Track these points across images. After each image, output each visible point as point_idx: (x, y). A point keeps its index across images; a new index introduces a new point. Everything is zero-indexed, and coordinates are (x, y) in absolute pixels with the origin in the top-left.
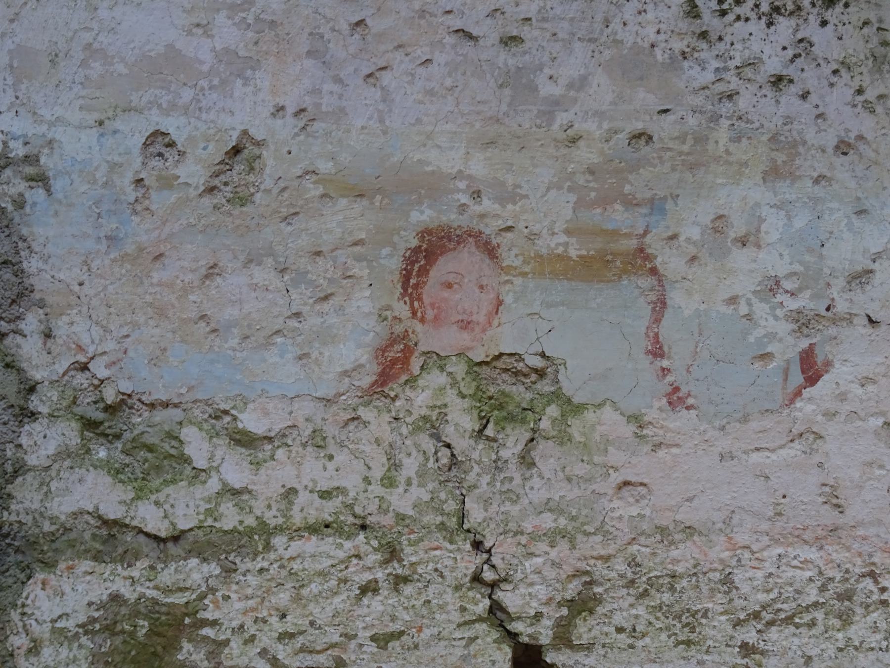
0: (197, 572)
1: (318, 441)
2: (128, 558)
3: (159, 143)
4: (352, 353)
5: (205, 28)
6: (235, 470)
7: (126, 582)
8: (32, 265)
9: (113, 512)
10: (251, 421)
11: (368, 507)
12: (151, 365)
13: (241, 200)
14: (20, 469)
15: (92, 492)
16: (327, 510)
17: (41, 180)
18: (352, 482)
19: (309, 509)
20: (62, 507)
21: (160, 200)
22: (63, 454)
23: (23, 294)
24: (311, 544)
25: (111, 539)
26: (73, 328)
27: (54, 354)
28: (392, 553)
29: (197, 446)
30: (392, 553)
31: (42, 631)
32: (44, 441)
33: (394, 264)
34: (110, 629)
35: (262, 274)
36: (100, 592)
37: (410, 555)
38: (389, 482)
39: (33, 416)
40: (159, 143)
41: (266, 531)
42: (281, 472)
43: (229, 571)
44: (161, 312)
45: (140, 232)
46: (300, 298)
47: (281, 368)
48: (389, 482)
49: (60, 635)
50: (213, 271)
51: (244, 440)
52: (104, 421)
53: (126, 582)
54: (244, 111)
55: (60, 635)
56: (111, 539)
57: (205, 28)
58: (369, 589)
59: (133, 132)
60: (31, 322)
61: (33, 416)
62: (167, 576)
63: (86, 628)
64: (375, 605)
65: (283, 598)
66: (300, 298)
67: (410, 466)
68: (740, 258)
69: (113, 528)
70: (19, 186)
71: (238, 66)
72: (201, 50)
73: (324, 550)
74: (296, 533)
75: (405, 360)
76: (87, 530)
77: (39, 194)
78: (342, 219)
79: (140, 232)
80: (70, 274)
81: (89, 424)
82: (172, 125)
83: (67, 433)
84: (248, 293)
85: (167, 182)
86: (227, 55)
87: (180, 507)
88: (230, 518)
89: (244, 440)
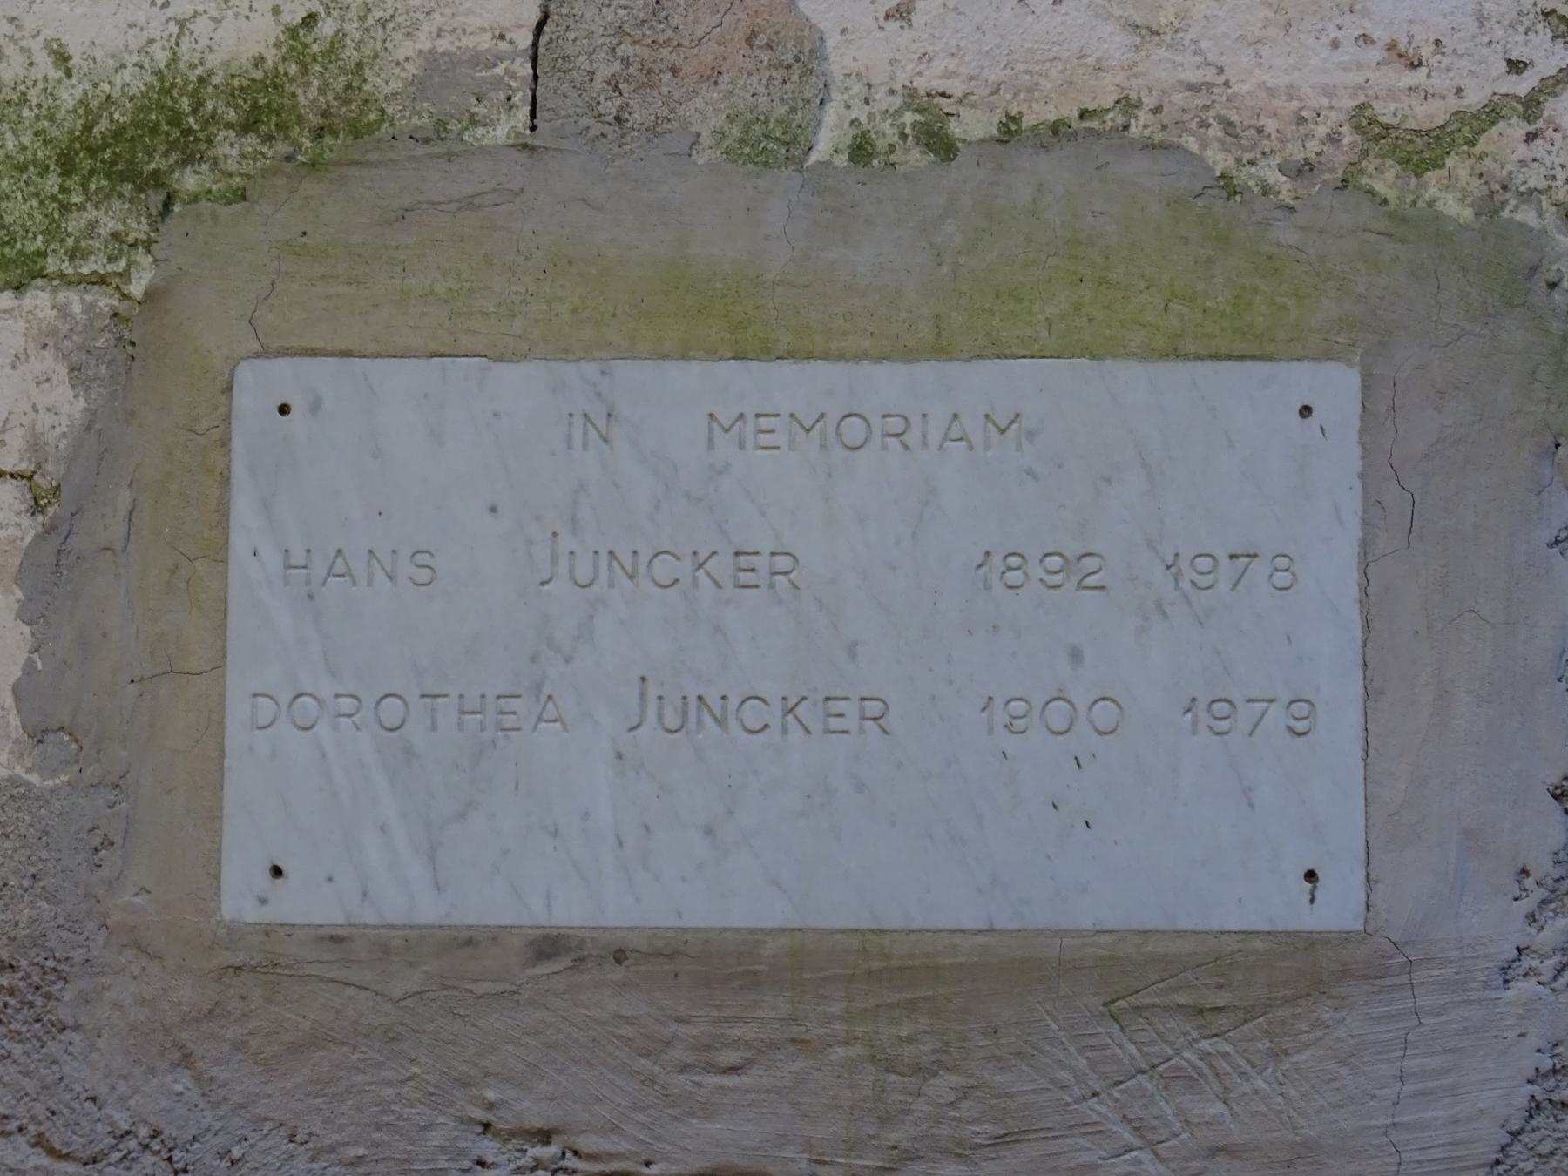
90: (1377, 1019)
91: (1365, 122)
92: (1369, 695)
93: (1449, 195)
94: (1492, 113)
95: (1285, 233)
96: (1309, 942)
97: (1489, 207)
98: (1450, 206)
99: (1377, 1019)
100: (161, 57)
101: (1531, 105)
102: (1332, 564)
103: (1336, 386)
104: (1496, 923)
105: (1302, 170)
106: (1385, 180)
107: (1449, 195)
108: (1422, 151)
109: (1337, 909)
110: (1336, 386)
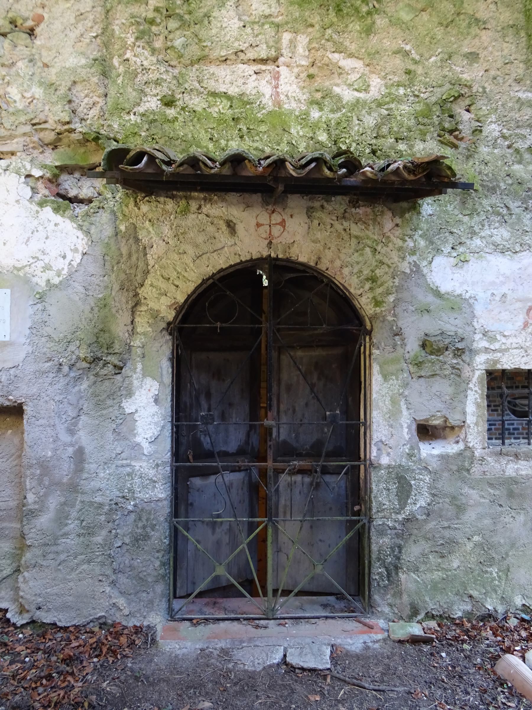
0: (499, 355)
1: (515, 336)
2: (489, 353)
3: (493, 294)
4: (520, 323)
5: (498, 278)
6: (504, 340)
7: (489, 356)
8: (475, 312)
9: (487, 347)
10: (506, 333)
11: (523, 345)
12: (492, 326)
13: (504, 302)
14: (474, 341)
15: (484, 344)
16: (517, 346)
17: (476, 300)
18: (520, 342)
19: (515, 345)
20: (480, 346)
21: (493, 302)
22: (480, 338)
23: (474, 316)
24: (515, 350)
25: (487, 350)
26: (481, 321)
27: (19, 198)
28: (526, 351)
29: (498, 337)
30: (526, 351)
31: (478, 363)
32: (477, 337)
33: (525, 311)
34: (487, 363)
35: (507, 313)
36: (486, 358)
37: (529, 352)
38: (525, 342)
39: (475, 333)
40: (493, 294)
41: (508, 349)
42: (510, 340)
43: (503, 354)
44: (493, 318)
45: (490, 307)
46: (512, 316)
47: (510, 326)
48: (525, 342)
49: (481, 364)
50: (500, 312)
51: (505, 336)
52: (485, 334)
53: (489, 356)
54: (504, 290)
55: (481, 364)
56: (487, 350)
57: (498, 278)
58: (523, 356)
59: (489, 293)
60: (475, 320)
61: (475, 333)
62: (495, 355)
63: (484, 363)
64: (524, 359)
65: (511, 358)
66: (512, 316)
67: (528, 339)
68: (20, 96)
69: (486, 349)
70: (473, 301)
71: (503, 283)
72: (497, 281)
73: (517, 351)
74: (513, 349)
75: (527, 325)
76: (483, 349)
77: (476, 302)
78: (518, 305)
79: (490, 307)
80: (480, 313)
81: (484, 334)
82: (495, 292)
83: (481, 336)
84: (505, 315)
85: (494, 300)
86: (501, 282)
87: (496, 346)
88: (503, 347)
89: (505, 336)
90: (128, 465)
91: (14, 266)
92: (11, 319)
93: (21, 274)
94: (26, 266)
95: (5, 277)
96: (4, 342)
97: (25, 275)
98: (21, 275)
99: (128, 465)
100: (147, 198)
101: (30, 265)
102: (7, 306)
103: (8, 291)
104: (23, 340)
105: (8, 271)
106: (15, 272)
107: (21, 274)
108: (19, 269)
109: (7, 339)
110: (8, 291)
